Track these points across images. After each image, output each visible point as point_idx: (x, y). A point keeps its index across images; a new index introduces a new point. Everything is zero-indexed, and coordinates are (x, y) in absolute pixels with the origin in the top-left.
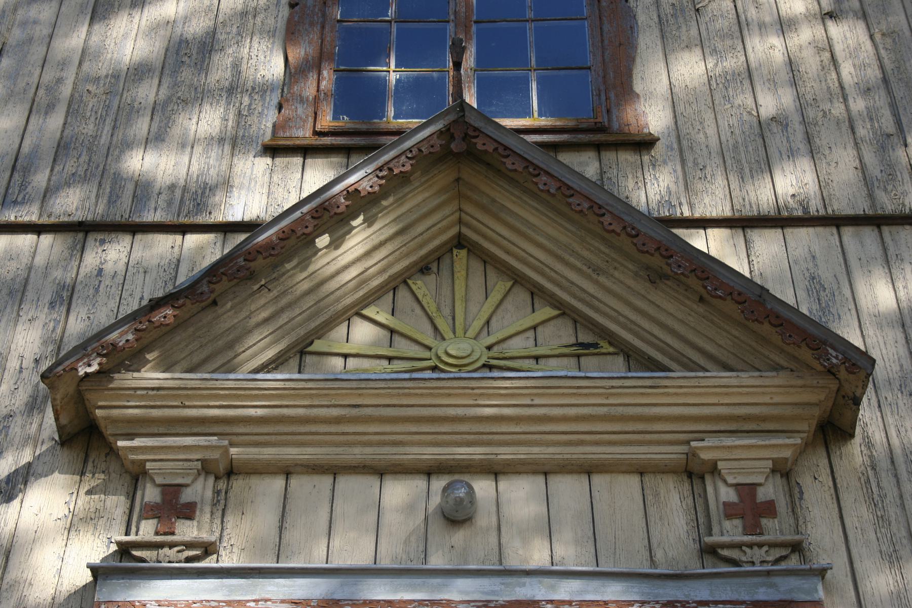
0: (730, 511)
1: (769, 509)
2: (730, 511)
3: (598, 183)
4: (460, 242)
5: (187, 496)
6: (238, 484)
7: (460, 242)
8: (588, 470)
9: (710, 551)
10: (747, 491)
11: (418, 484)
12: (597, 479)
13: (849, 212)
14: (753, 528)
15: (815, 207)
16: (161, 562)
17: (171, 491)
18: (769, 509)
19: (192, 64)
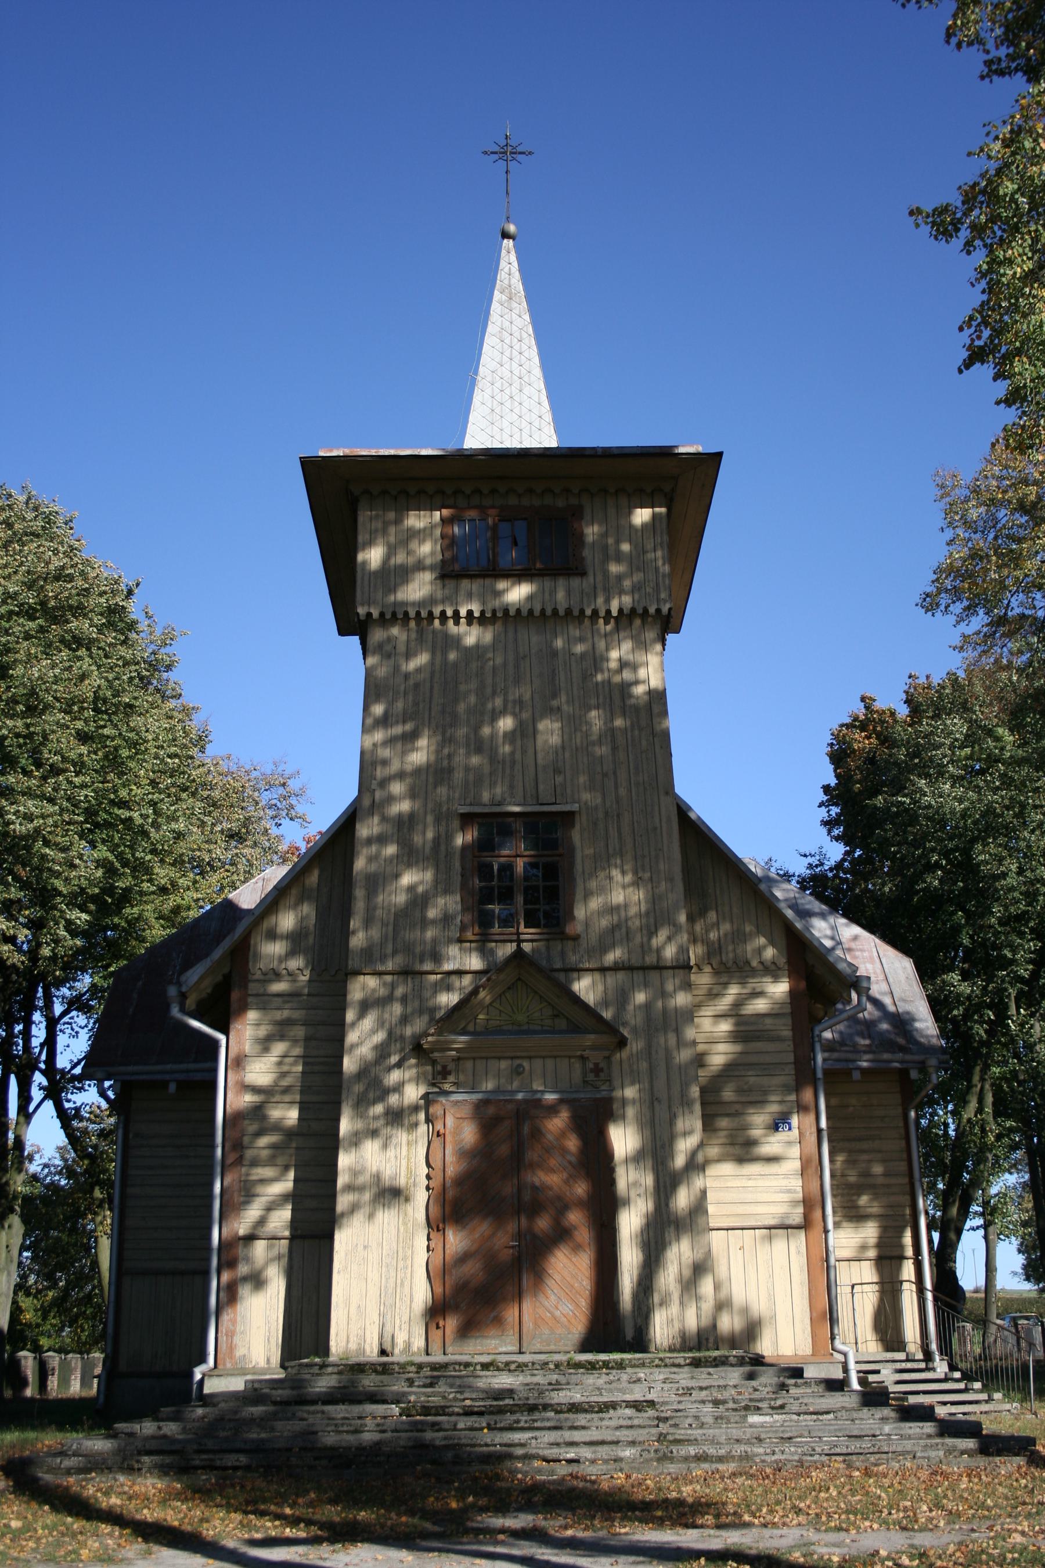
0: (592, 1071)
1: (602, 1070)
2: (592, 1071)
3: (607, 1014)
4: (519, 979)
5: (449, 1068)
6: (461, 1062)
7: (519, 979)
8: (555, 1057)
9: (585, 1082)
10: (596, 1065)
11: (509, 1062)
12: (558, 1060)
13: (636, 965)
14: (597, 1075)
15: (626, 965)
16: (413, 1416)
17: (444, 1067)
18: (602, 1070)
19: (285, 1068)
